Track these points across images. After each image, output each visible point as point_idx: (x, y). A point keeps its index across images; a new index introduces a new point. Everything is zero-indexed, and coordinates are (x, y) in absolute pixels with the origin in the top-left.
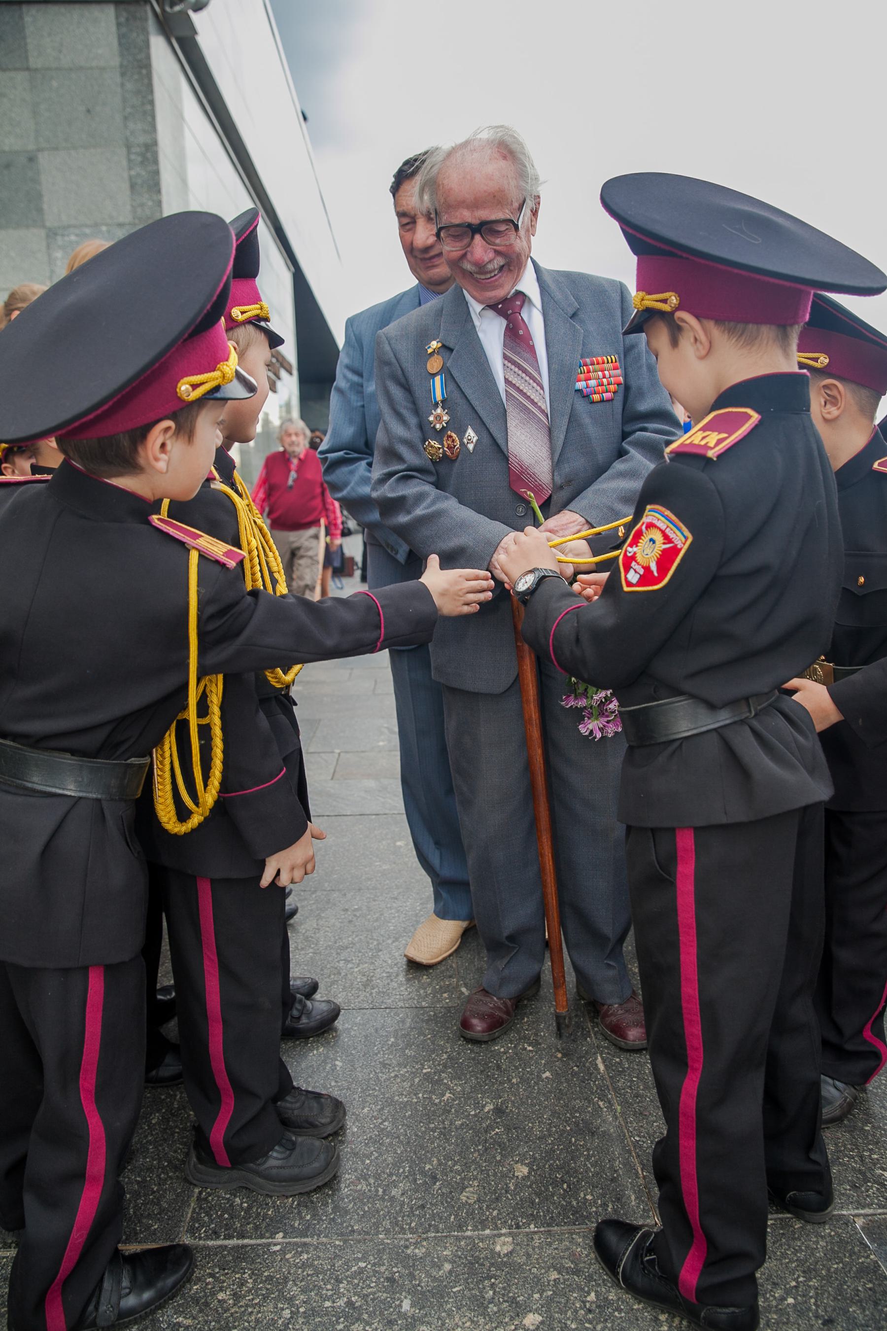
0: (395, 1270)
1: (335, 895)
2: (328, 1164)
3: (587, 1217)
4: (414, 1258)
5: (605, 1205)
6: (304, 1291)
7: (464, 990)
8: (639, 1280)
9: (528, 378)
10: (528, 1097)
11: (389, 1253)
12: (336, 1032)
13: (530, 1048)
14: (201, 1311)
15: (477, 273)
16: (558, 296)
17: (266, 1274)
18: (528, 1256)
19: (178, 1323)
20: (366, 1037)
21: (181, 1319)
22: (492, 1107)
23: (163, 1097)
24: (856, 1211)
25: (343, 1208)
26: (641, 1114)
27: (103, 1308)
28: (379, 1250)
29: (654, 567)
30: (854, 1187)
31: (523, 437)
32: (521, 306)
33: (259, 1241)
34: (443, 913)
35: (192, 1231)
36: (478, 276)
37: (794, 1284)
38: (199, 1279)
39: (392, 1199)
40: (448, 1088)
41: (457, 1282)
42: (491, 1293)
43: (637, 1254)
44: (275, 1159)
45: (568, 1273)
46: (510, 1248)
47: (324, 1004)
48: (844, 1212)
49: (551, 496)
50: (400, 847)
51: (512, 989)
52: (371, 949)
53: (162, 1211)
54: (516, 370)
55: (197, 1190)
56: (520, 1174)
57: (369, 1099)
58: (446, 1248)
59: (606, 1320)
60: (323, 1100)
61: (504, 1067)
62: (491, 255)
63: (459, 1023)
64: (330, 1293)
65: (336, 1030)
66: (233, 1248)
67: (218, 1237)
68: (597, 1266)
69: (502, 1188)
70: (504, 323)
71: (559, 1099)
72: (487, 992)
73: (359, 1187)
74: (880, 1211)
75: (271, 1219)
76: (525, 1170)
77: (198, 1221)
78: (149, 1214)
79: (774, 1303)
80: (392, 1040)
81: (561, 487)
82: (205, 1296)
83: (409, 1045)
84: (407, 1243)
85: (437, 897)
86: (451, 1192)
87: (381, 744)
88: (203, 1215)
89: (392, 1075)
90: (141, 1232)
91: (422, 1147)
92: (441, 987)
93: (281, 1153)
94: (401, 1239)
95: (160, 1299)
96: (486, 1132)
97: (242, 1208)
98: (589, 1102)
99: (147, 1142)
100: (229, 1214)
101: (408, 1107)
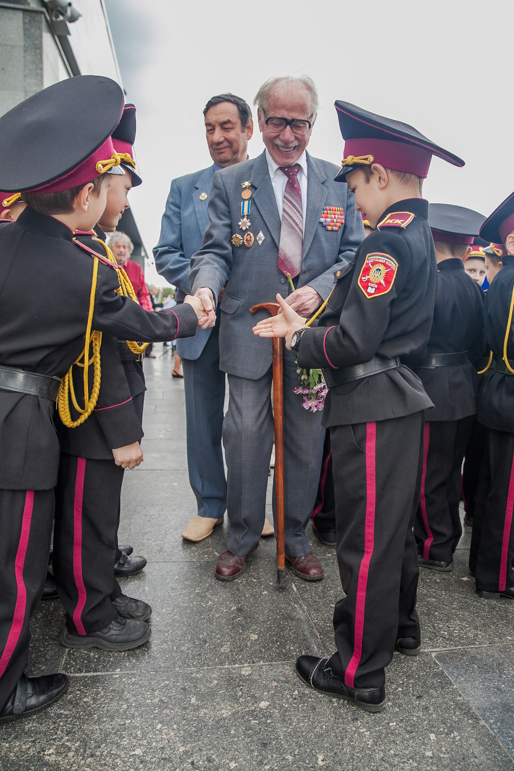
0: (186, 684)
1: (139, 508)
2: (145, 633)
3: (291, 657)
4: (197, 679)
5: (301, 651)
6: (134, 696)
7: (216, 553)
8: (322, 682)
9: (295, 211)
10: (255, 603)
11: (182, 677)
12: (144, 573)
13: (255, 580)
14: (74, 707)
15: (282, 147)
16: (316, 171)
17: (111, 688)
18: (260, 675)
19: (61, 713)
20: (162, 575)
21: (62, 711)
22: (235, 608)
23: (43, 605)
24: (432, 650)
25: (154, 657)
26: (318, 610)
27: (16, 703)
28: (176, 676)
29: (383, 282)
30: (430, 639)
31: (288, 241)
32: (297, 172)
33: (106, 673)
34: (203, 514)
35: (66, 669)
36: (283, 149)
37: (402, 682)
38: (72, 692)
39: (182, 652)
40: (210, 599)
41: (221, 689)
42: (241, 693)
43: (320, 670)
44: (114, 630)
45: (282, 682)
46: (250, 672)
47: (138, 558)
48: (426, 650)
49: (298, 275)
50: (175, 486)
51: (244, 552)
52: (161, 534)
53: (47, 660)
54: (290, 205)
55: (67, 650)
56: (253, 639)
57: (165, 605)
58: (214, 673)
59: (304, 703)
60: (139, 603)
61: (241, 589)
62: (294, 138)
63: (215, 570)
64: (149, 696)
65: (144, 573)
66: (91, 677)
67: (81, 672)
68: (298, 679)
69: (244, 645)
70: (287, 179)
71: (273, 604)
72: (231, 553)
73: (163, 646)
74: (444, 649)
75: (113, 663)
76: (256, 637)
77: (69, 664)
78: (39, 662)
79: (392, 691)
80: (177, 577)
81: (305, 272)
82: (76, 699)
83: (186, 579)
84: (192, 672)
85: (200, 505)
86: (215, 648)
87: (161, 436)
88: (72, 661)
89: (178, 593)
90: (35, 671)
91: (197, 627)
92: (203, 552)
93: (118, 627)
94: (188, 670)
95: (50, 700)
96: (233, 619)
97: (95, 658)
98: (289, 605)
99: (35, 627)
100: (87, 661)
101: (188, 609)
